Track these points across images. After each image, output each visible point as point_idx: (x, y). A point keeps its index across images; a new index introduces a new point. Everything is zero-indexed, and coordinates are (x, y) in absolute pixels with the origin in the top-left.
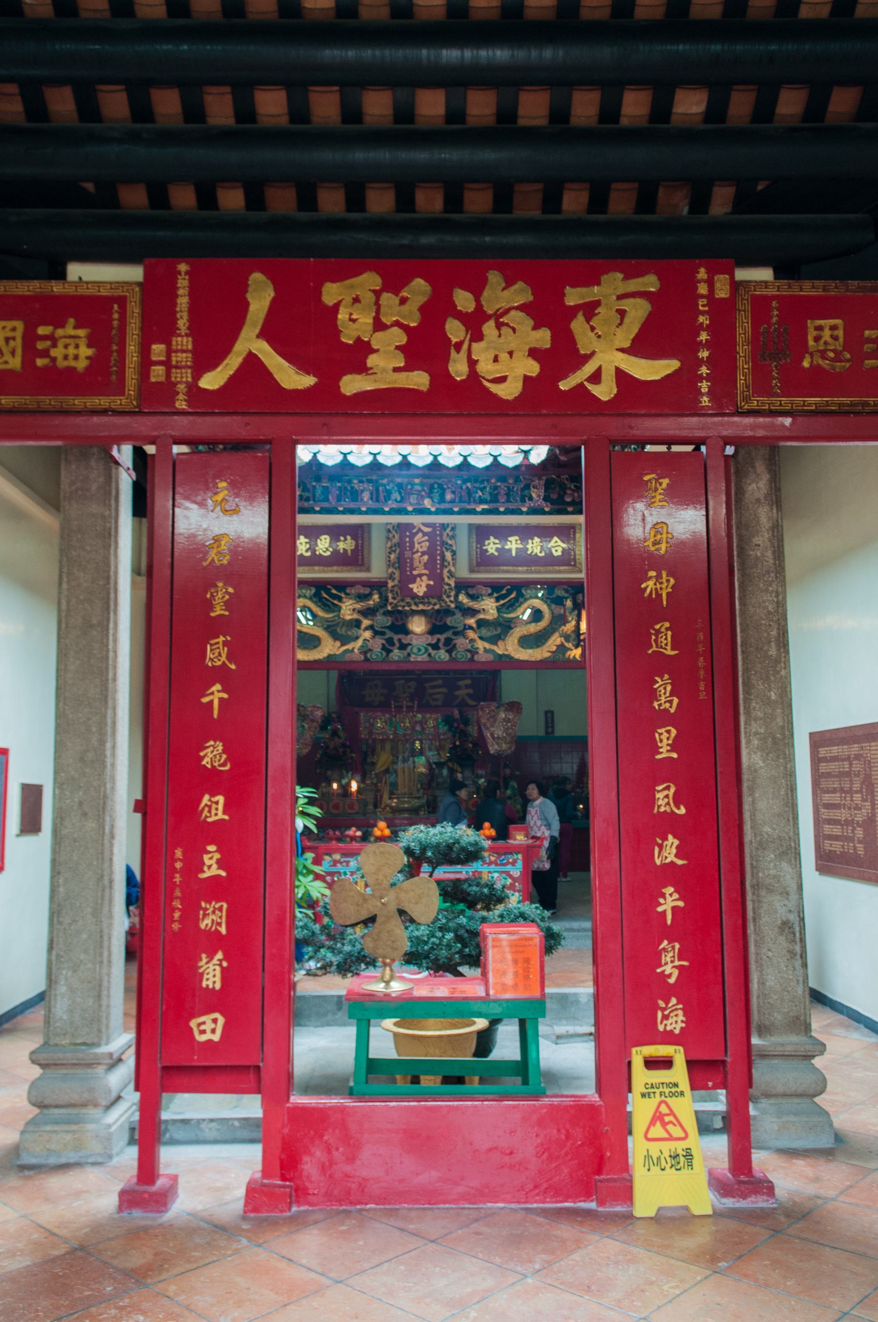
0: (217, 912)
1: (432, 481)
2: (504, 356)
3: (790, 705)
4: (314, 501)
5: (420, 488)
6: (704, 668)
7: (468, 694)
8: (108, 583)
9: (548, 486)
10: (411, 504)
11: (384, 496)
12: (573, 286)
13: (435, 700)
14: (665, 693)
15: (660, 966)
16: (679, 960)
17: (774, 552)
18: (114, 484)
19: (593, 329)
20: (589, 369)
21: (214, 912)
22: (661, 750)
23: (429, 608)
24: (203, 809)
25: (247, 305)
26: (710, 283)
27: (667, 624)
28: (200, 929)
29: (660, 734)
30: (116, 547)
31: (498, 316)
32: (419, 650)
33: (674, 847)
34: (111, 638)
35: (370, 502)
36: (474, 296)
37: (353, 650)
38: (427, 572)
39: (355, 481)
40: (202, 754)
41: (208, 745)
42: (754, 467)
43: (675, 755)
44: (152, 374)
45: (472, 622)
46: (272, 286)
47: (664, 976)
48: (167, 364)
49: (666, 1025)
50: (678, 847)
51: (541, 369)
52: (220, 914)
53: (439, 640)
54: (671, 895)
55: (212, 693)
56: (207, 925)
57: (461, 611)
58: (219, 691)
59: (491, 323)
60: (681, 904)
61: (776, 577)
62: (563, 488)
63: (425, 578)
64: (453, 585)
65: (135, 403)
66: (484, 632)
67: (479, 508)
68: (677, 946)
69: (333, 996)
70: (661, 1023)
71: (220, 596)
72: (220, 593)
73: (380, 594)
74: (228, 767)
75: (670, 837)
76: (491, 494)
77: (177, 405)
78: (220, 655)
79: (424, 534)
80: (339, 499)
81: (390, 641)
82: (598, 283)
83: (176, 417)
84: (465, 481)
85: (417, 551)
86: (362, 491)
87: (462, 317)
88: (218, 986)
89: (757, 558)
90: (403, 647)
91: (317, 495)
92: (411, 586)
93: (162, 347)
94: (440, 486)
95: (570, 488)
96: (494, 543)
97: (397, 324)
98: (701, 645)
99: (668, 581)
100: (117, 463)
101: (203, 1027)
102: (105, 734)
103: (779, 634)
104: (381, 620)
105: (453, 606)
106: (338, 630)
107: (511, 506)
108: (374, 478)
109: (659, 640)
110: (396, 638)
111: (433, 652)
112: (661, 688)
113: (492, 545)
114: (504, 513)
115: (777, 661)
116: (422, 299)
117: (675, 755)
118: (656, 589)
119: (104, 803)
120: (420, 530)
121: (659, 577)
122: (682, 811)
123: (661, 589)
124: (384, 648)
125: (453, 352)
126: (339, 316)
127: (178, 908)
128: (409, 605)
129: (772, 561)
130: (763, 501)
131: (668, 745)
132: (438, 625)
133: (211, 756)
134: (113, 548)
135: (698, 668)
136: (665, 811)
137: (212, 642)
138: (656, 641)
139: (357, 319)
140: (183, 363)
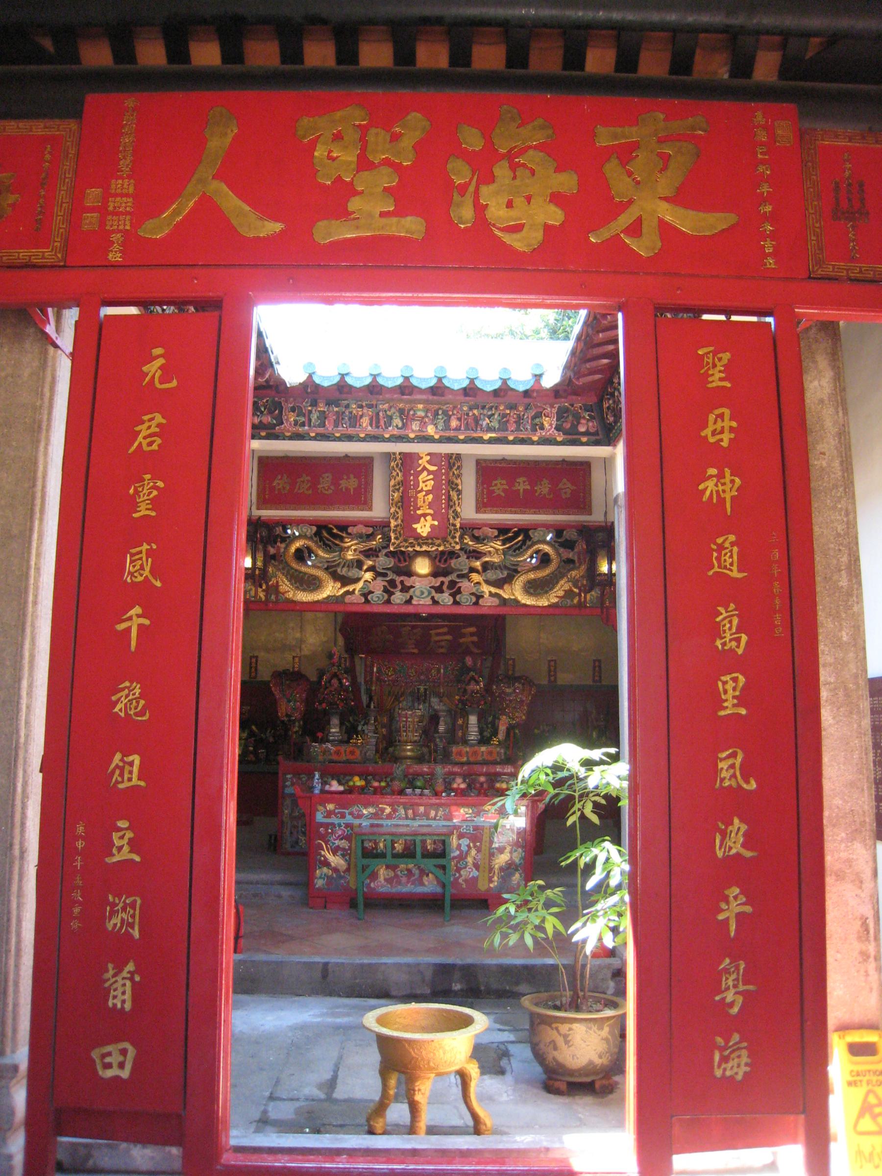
1: (437, 407)
2: (519, 201)
3: (864, 649)
4: (310, 426)
5: (423, 414)
7: (473, 642)
8: (34, 486)
9: (561, 414)
10: (413, 431)
12: (605, 125)
14: (730, 629)
15: (720, 992)
16: (745, 983)
17: (842, 463)
18: (49, 370)
19: (630, 174)
20: (625, 220)
21: (124, 909)
22: (725, 704)
23: (433, 549)
24: (113, 772)
25: (203, 142)
26: (770, 130)
27: (732, 538)
28: (105, 929)
29: (724, 683)
30: (47, 445)
31: (510, 156)
32: (422, 593)
33: (741, 833)
34: (34, 552)
35: (369, 428)
37: (353, 592)
38: (431, 511)
40: (114, 698)
42: (815, 362)
45: (478, 564)
47: (725, 1005)
49: (725, 1070)
50: (745, 835)
52: (132, 912)
53: (442, 583)
54: (736, 898)
55: (130, 618)
56: (115, 925)
57: (466, 552)
58: (138, 616)
59: (505, 163)
60: (748, 909)
61: (846, 492)
63: (429, 518)
64: (458, 526)
65: (59, 256)
66: (491, 575)
68: (742, 965)
69: (319, 963)
70: (719, 1066)
72: (146, 488)
73: (383, 534)
75: (736, 821)
76: (499, 422)
77: (110, 256)
78: (142, 568)
79: (430, 473)
81: (392, 583)
82: (636, 123)
84: (471, 409)
85: (422, 490)
86: (361, 416)
87: (469, 157)
88: (128, 1006)
89: (822, 469)
90: (405, 589)
91: (313, 420)
92: (415, 526)
94: (445, 413)
95: (584, 418)
96: (502, 485)
97: (387, 162)
98: (775, 566)
100: (56, 346)
101: (108, 1060)
102: (21, 669)
103: (850, 561)
104: (383, 561)
105: (458, 547)
106: (339, 570)
107: (522, 436)
108: (374, 402)
109: (723, 558)
110: (398, 579)
112: (726, 622)
114: (513, 442)
115: (849, 594)
116: (418, 135)
117: (743, 712)
118: (718, 492)
120: (425, 469)
121: (720, 476)
122: (753, 785)
123: (724, 491)
124: (386, 590)
125: (456, 197)
126: (316, 154)
127: (78, 902)
129: (840, 474)
130: (826, 402)
131: (734, 697)
132: (443, 564)
134: (42, 444)
136: (730, 786)
137: (133, 551)
138: (718, 559)
139: (337, 157)
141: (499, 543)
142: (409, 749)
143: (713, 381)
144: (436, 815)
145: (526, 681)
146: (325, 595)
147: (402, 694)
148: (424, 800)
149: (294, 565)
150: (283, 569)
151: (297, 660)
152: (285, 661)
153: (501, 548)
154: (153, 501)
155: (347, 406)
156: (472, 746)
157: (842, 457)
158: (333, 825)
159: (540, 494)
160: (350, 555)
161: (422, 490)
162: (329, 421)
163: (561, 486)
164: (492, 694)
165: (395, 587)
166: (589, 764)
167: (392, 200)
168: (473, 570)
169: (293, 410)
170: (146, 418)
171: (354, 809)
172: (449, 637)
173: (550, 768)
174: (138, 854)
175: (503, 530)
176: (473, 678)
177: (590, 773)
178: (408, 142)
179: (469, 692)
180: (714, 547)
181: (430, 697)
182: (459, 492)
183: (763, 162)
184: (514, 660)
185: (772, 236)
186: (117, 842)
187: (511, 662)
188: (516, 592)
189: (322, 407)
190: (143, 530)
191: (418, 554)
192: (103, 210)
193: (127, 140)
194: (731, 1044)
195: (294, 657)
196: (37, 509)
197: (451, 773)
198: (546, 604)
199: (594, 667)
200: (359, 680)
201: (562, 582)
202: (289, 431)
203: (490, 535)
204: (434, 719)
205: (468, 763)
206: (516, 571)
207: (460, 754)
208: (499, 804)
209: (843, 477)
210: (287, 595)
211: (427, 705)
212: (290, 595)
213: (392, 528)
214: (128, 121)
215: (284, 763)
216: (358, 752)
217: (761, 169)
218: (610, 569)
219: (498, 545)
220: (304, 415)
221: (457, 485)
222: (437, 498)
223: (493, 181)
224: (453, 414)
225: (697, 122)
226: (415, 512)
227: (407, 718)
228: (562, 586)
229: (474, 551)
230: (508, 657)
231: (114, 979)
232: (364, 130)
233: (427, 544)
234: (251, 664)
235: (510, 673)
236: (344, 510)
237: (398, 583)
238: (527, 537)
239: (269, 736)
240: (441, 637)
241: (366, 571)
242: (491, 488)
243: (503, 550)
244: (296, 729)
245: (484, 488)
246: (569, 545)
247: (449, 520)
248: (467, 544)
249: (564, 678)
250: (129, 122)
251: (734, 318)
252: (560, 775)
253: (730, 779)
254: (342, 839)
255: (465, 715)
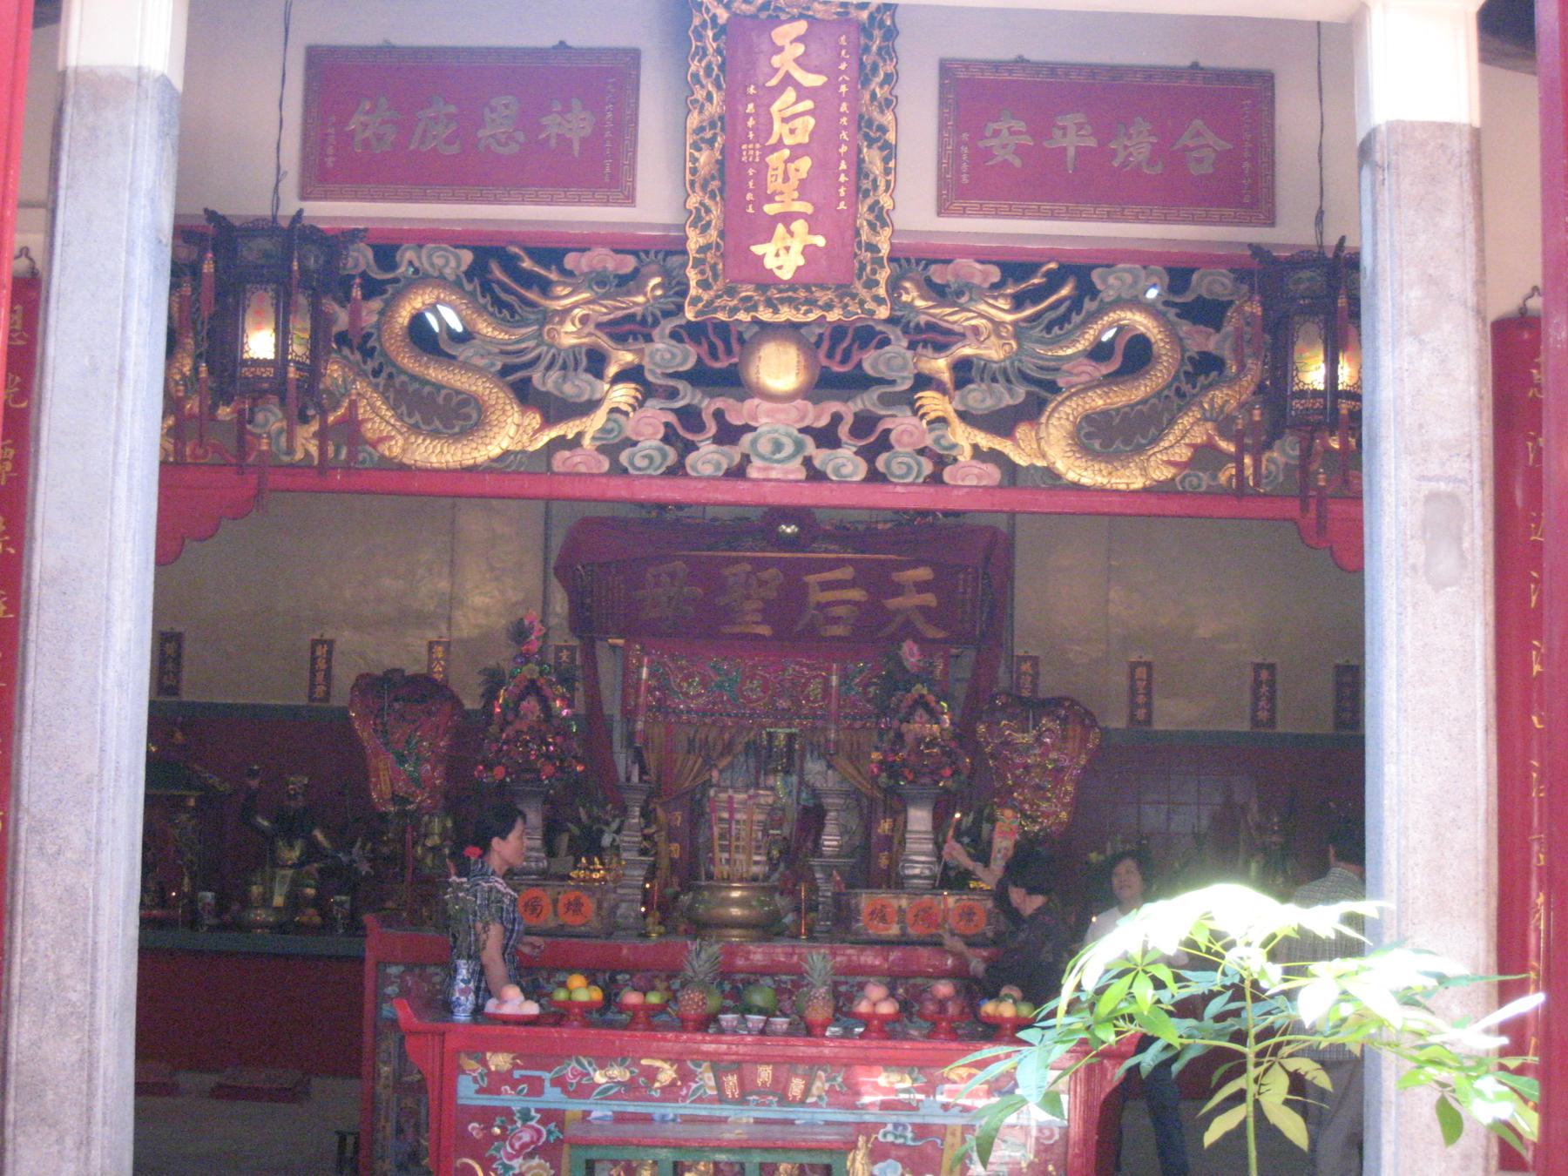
7: (923, 609)
13: (836, 620)
23: (812, 317)
32: (778, 447)
37: (576, 442)
38: (806, 207)
45: (940, 365)
53: (837, 419)
57: (906, 332)
63: (799, 226)
64: (885, 250)
66: (979, 397)
73: (666, 274)
79: (803, 93)
81: (690, 418)
85: (780, 145)
90: (728, 434)
92: (757, 249)
96: (1012, 133)
105: (883, 312)
106: (537, 377)
110: (708, 406)
120: (788, 80)
124: (669, 437)
132: (839, 365)
141: (1002, 303)
142: (736, 901)
144: (807, 1091)
145: (1072, 712)
146: (495, 451)
147: (728, 748)
148: (772, 1047)
149: (408, 361)
150: (376, 373)
151: (439, 651)
152: (408, 653)
153: (1009, 318)
156: (917, 892)
158: (507, 1113)
159: (1124, 164)
160: (569, 335)
161: (780, 145)
163: (1186, 140)
164: (976, 750)
165: (700, 427)
166: (1295, 952)
168: (924, 381)
171: (570, 1069)
172: (856, 594)
173: (1170, 962)
175: (1014, 270)
176: (921, 702)
177: (1297, 982)
179: (909, 739)
181: (803, 757)
184: (1035, 661)
187: (1026, 667)
188: (1050, 447)
191: (768, 331)
195: (431, 645)
197: (853, 970)
198: (1138, 483)
199: (1257, 683)
200: (607, 712)
201: (1186, 421)
203: (976, 280)
204: (812, 819)
205: (902, 942)
206: (1053, 388)
207: (880, 914)
208: (996, 1070)
210: (384, 449)
211: (794, 779)
212: (395, 449)
213: (692, 253)
215: (378, 937)
216: (590, 904)
218: (1332, 377)
219: (1000, 310)
221: (883, 129)
222: (824, 167)
226: (758, 208)
227: (732, 811)
228: (1185, 433)
229: (931, 327)
230: (1019, 652)
233: (792, 302)
234: (314, 660)
235: (1026, 694)
236: (551, 202)
238: (1087, 289)
239: (359, 859)
240: (835, 592)
241: (617, 379)
242: (981, 144)
243: (1015, 324)
244: (433, 841)
245: (959, 144)
246: (1208, 313)
247: (857, 233)
248: (910, 305)
249: (1174, 713)
252: (1200, 983)
254: (531, 1156)
255: (896, 806)
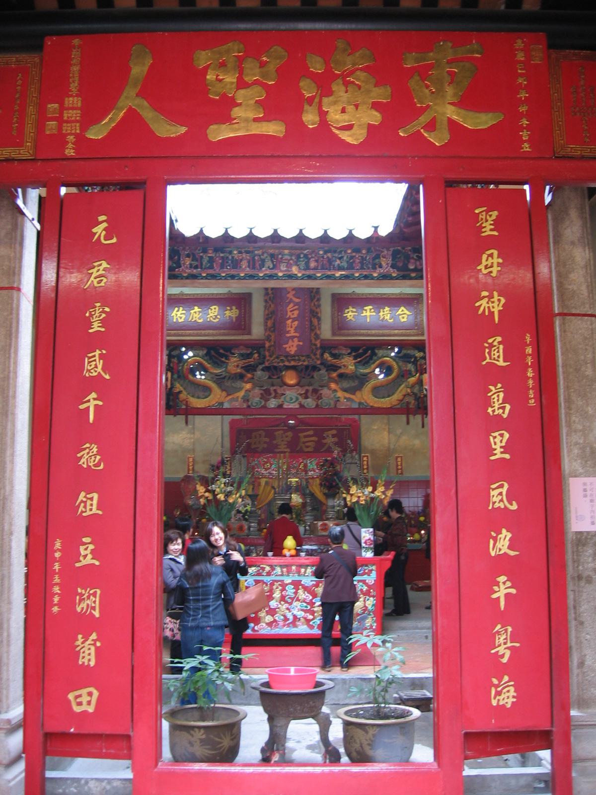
0: (91, 597)
2: (350, 108)
4: (201, 268)
5: (289, 258)
6: (533, 378)
8: (11, 314)
9: (395, 255)
10: (281, 271)
11: (260, 265)
13: (307, 447)
17: (588, 286)
20: (424, 119)
21: (88, 597)
22: (495, 452)
27: (499, 339)
28: (76, 611)
29: (495, 437)
31: (344, 76)
32: (291, 399)
36: (325, 60)
38: (297, 334)
39: (235, 252)
40: (79, 455)
41: (84, 447)
43: (507, 456)
44: (47, 128)
45: (334, 375)
46: (151, 55)
48: (60, 120)
49: (499, 700)
51: (383, 117)
52: (94, 599)
53: (307, 391)
54: (504, 583)
56: (83, 608)
57: (325, 366)
58: (95, 399)
59: (340, 81)
60: (513, 591)
62: (408, 258)
63: (296, 339)
64: (319, 345)
66: (346, 385)
67: (338, 274)
68: (510, 629)
70: (495, 698)
71: (97, 314)
72: (97, 312)
74: (102, 467)
75: (504, 531)
76: (347, 262)
77: (67, 152)
78: (96, 366)
80: (222, 266)
81: (267, 392)
83: (65, 162)
84: (326, 252)
85: (289, 318)
86: (241, 260)
87: (314, 77)
88: (92, 663)
89: (574, 292)
91: (204, 263)
93: (56, 106)
95: (413, 258)
97: (257, 82)
99: (499, 300)
100: (22, 213)
101: (79, 700)
105: (319, 362)
108: (251, 249)
109: (492, 353)
111: (303, 401)
112: (495, 396)
113: (350, 313)
118: (489, 307)
119: (4, 504)
120: (291, 301)
121: (491, 297)
122: (514, 507)
123: (493, 307)
125: (306, 107)
126: (208, 77)
128: (282, 361)
131: (501, 447)
133: (86, 457)
135: (528, 389)
137: (90, 355)
138: (489, 353)
140: (73, 119)
143: (485, 232)
154: (102, 321)
155: (230, 252)
157: (588, 282)
162: (217, 264)
167: (261, 110)
169: (188, 256)
170: (96, 264)
174: (97, 560)
178: (272, 68)
180: (486, 345)
182: (319, 319)
183: (522, 75)
185: (528, 128)
186: (83, 552)
189: (211, 254)
190: (97, 341)
192: (60, 120)
193: (75, 69)
194: (502, 683)
196: (14, 330)
202: (185, 273)
209: (589, 297)
214: (75, 55)
217: (520, 80)
220: (197, 261)
223: (331, 95)
224: (312, 257)
225: (474, 49)
229: (332, 365)
231: (83, 645)
232: (240, 60)
237: (272, 392)
250: (76, 54)
251: (501, 187)
253: (499, 503)
